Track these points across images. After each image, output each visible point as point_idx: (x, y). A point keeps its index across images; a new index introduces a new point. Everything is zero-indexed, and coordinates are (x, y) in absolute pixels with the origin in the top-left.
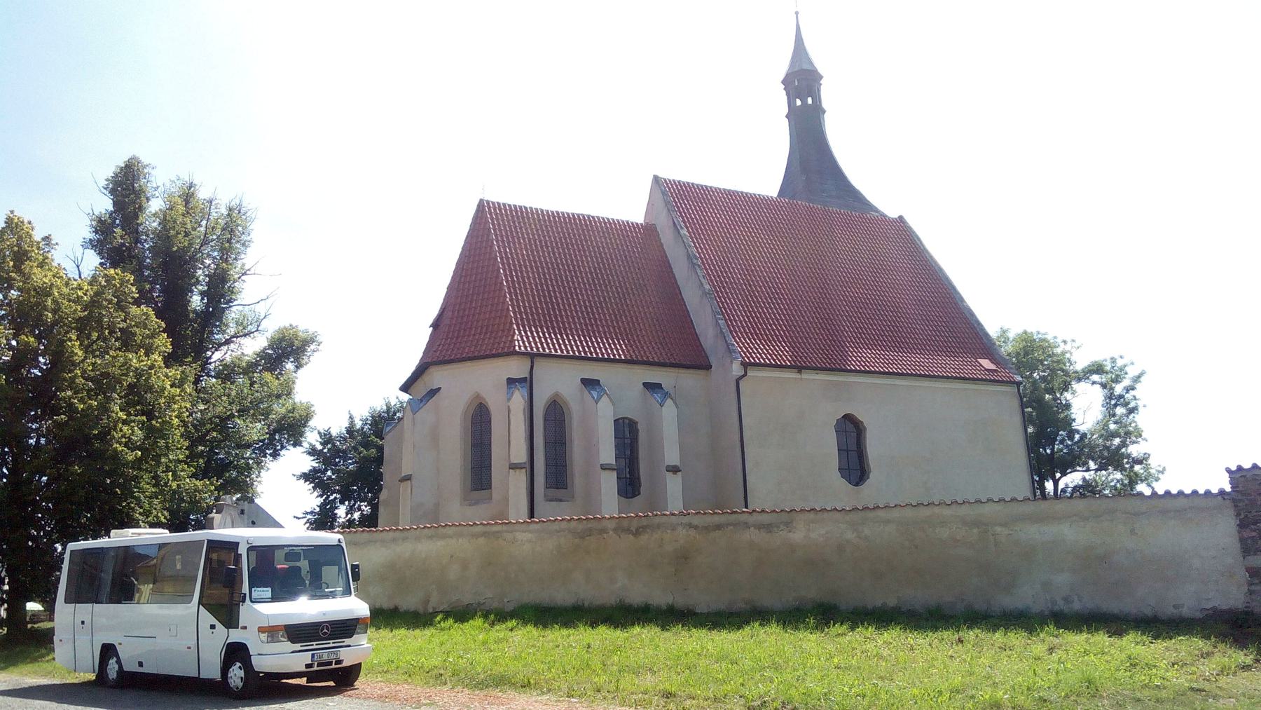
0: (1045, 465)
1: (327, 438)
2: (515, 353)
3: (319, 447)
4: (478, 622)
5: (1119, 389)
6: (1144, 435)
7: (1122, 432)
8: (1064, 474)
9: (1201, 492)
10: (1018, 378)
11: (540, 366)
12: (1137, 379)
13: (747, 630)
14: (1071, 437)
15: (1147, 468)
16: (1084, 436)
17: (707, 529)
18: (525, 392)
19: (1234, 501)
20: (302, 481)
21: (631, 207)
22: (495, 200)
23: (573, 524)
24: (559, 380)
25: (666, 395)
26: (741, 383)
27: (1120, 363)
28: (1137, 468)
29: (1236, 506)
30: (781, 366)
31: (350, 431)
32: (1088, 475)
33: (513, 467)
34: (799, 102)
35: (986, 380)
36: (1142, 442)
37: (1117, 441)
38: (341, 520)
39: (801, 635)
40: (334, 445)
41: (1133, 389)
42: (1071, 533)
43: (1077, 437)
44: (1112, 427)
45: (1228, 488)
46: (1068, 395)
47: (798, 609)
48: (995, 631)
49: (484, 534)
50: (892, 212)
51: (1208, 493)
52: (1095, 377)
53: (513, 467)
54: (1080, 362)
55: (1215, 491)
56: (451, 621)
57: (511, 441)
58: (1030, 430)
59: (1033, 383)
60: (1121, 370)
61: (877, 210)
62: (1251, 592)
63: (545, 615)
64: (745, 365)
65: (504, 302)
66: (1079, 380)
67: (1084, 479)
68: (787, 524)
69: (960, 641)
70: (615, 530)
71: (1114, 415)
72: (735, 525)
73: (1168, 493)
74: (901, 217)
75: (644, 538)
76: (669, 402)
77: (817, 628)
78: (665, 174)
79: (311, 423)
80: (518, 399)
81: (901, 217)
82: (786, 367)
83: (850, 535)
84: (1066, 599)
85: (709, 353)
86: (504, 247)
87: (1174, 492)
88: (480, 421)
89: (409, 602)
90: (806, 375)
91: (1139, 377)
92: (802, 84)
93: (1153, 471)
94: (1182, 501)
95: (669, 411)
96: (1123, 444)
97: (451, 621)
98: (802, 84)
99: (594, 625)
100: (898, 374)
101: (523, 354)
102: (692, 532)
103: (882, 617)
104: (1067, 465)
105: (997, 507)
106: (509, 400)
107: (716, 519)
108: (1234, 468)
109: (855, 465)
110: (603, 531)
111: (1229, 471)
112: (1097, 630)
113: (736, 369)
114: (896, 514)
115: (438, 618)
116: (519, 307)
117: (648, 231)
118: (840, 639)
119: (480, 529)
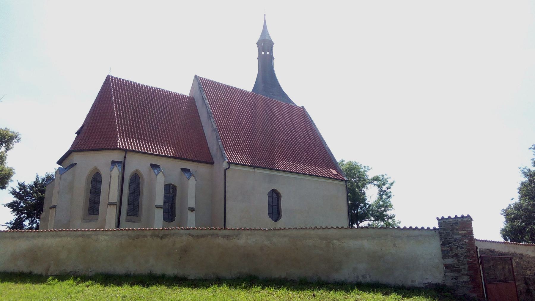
0: (355, 218)
1: (22, 186)
2: (117, 149)
3: (18, 190)
4: (71, 281)
5: (384, 188)
6: (393, 207)
7: (385, 205)
8: (361, 222)
9: (426, 228)
10: (346, 179)
11: (129, 156)
12: (391, 184)
13: (210, 289)
14: (365, 206)
15: (393, 221)
16: (370, 205)
17: (198, 237)
18: (120, 168)
19: (440, 233)
20: (7, 207)
21: (183, 88)
22: (116, 76)
23: (130, 232)
24: (137, 164)
25: (191, 174)
26: (227, 172)
27: (385, 177)
28: (390, 221)
29: (440, 235)
30: (246, 165)
31: (36, 183)
32: (370, 223)
33: (110, 204)
34: (263, 53)
35: (333, 178)
36: (393, 210)
37: (383, 209)
38: (26, 227)
39: (238, 291)
40: (25, 190)
41: (390, 188)
42: (366, 244)
43: (367, 206)
44: (381, 203)
45: (437, 227)
46: (365, 189)
47: (238, 278)
48: (330, 291)
49: (82, 236)
50: (299, 105)
51: (428, 228)
52: (376, 182)
53: (110, 204)
54: (370, 175)
55: (431, 228)
56: (56, 280)
57: (111, 191)
58: (349, 202)
59: (352, 181)
60: (386, 180)
61: (293, 103)
62: (445, 276)
63: (108, 279)
64: (229, 163)
65: (115, 124)
66: (370, 183)
67: (369, 224)
68: (237, 236)
69: (314, 296)
70: (151, 236)
71: (382, 199)
72: (212, 235)
73: (405, 228)
74: (303, 107)
75: (166, 240)
76: (192, 178)
77: (246, 288)
78: (200, 75)
79: (12, 178)
80: (116, 171)
81: (303, 107)
82: (248, 166)
83: (267, 242)
84: (364, 276)
85: (213, 157)
86: (118, 99)
87: (414, 227)
88: (96, 181)
89: (38, 270)
90: (258, 171)
91: (392, 183)
92: (265, 46)
93: (396, 222)
94: (416, 232)
95: (192, 183)
96: (385, 210)
97: (56, 280)
98: (265, 46)
99: (132, 284)
100: (297, 173)
101: (120, 149)
102: (190, 238)
103: (278, 283)
104: (363, 217)
105: (335, 231)
106: (111, 171)
107: (203, 232)
108: (440, 218)
109: (275, 212)
110: (146, 236)
111: (438, 219)
112: (377, 292)
113: (225, 165)
114: (288, 232)
115: (50, 279)
116: (122, 127)
117: (191, 100)
118: (256, 294)
119: (79, 233)
